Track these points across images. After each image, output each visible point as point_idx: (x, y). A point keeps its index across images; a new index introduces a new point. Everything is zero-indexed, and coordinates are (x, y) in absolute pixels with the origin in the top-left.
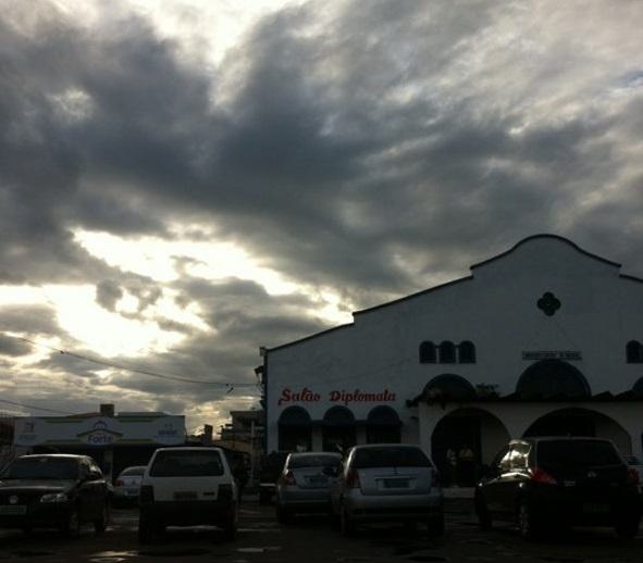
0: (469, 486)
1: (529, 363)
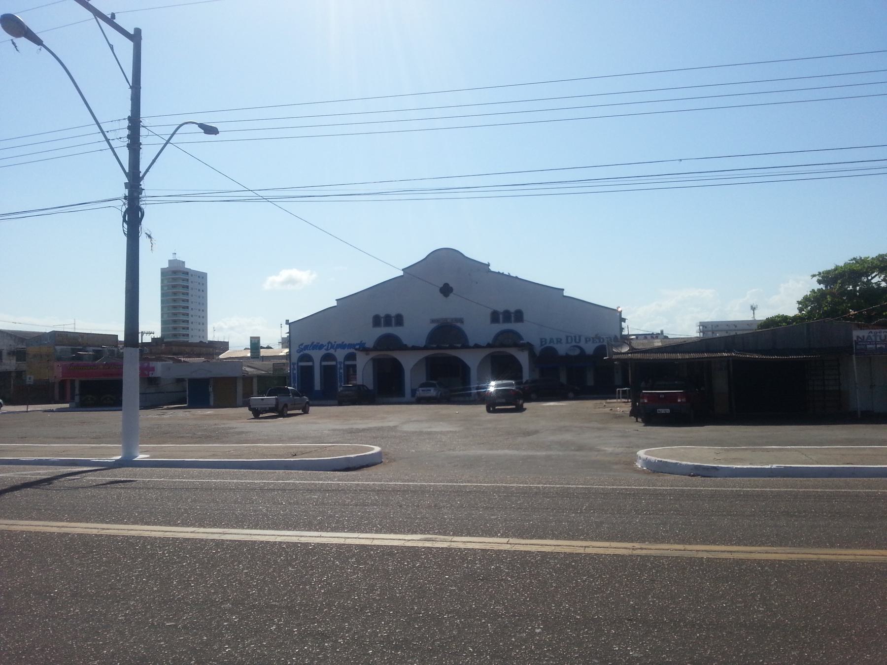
0: (333, 361)
1: (434, 325)
